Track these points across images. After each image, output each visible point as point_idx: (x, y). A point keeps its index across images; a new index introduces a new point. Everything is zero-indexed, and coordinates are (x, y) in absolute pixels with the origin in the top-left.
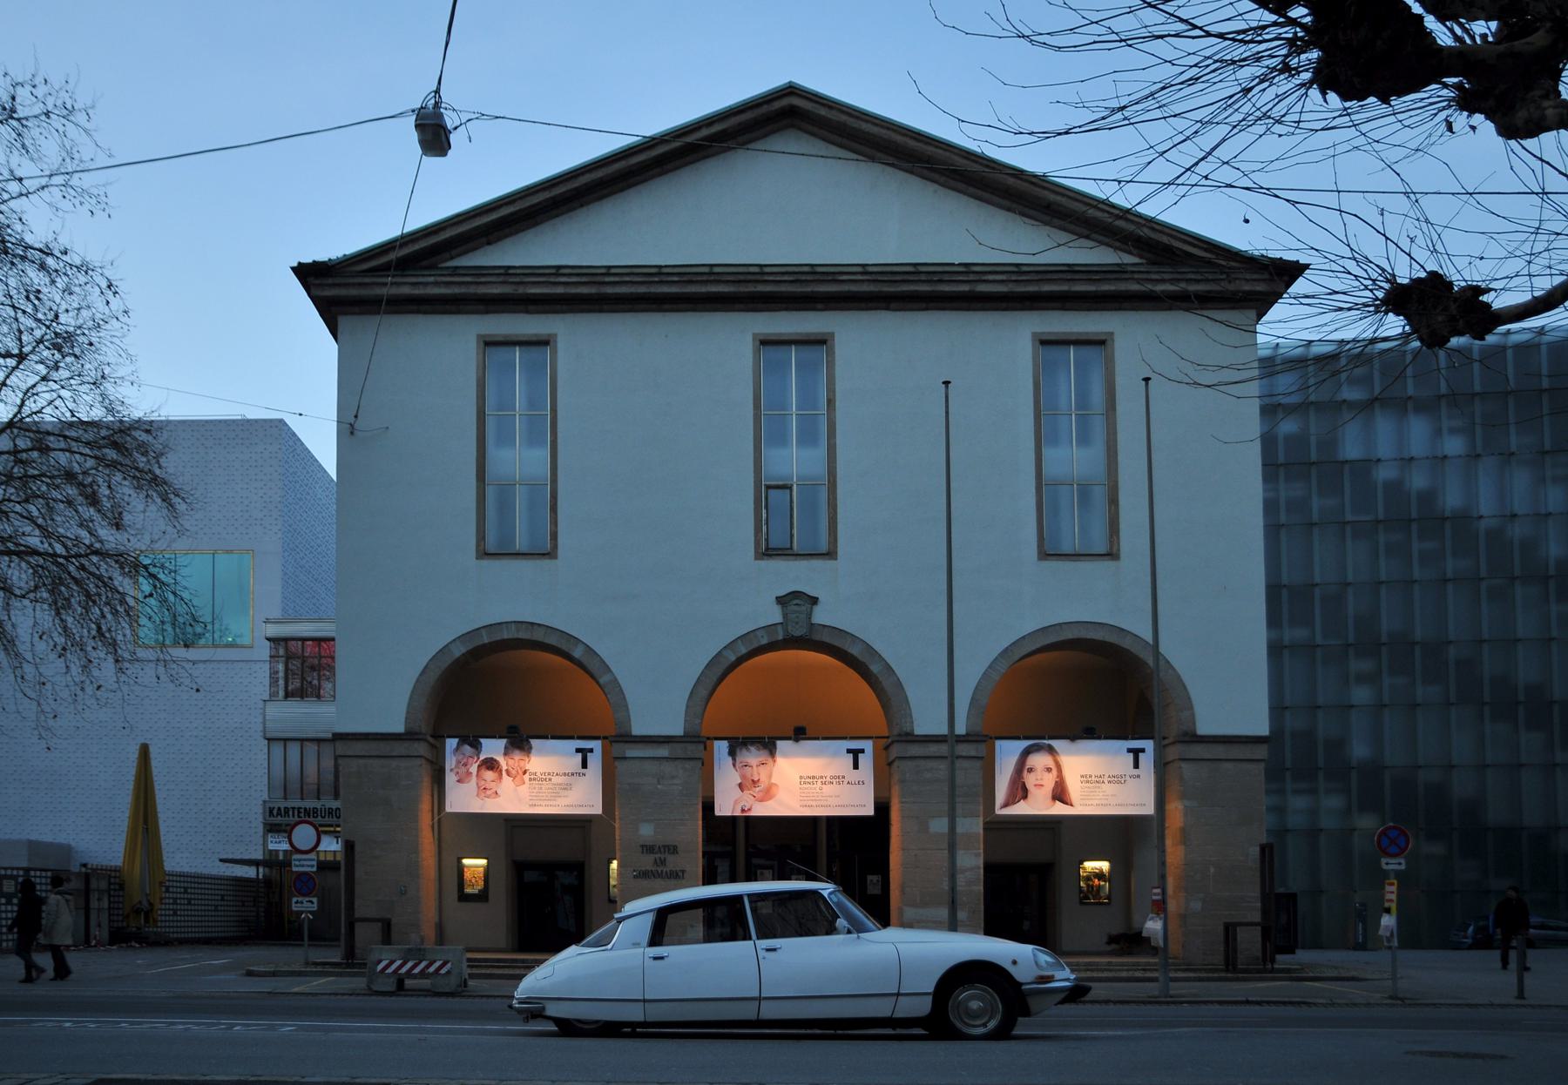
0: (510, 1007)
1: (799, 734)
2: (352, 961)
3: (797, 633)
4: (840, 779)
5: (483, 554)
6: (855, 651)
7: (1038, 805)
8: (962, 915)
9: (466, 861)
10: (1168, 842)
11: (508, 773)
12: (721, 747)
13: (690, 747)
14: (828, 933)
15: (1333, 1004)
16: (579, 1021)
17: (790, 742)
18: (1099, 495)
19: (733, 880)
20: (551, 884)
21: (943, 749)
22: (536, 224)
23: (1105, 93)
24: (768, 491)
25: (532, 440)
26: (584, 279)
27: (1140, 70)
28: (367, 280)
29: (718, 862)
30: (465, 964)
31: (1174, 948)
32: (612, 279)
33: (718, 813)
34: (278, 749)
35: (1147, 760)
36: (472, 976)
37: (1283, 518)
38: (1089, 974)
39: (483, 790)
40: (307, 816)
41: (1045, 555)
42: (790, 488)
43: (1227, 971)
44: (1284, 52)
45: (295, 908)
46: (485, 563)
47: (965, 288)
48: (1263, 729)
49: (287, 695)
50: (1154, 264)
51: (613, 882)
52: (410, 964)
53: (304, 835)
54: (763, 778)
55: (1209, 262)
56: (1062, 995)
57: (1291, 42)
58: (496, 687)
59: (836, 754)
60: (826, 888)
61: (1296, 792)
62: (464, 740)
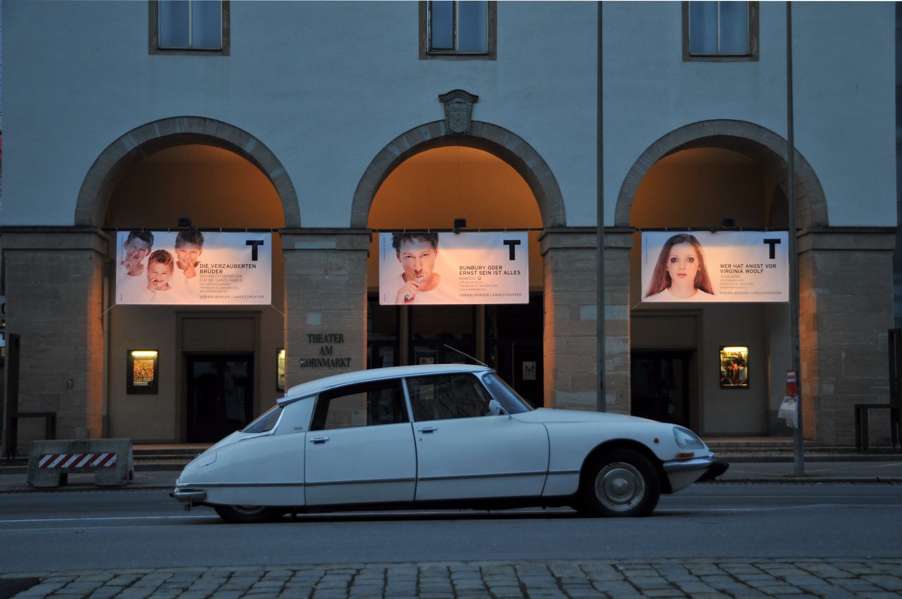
0: (172, 495)
1: (460, 226)
4: (497, 269)
5: (156, 49)
6: (512, 147)
7: (681, 293)
8: (610, 398)
9: (136, 354)
10: (802, 328)
11: (180, 265)
12: (386, 239)
13: (357, 239)
14: (483, 414)
17: (450, 235)
19: (397, 363)
20: (219, 377)
21: (592, 240)
30: (131, 456)
31: (809, 430)
33: (382, 302)
35: (782, 251)
36: (137, 468)
38: (729, 455)
39: (154, 282)
41: (689, 56)
46: (158, 58)
48: (891, 221)
51: (281, 371)
52: (74, 458)
54: (426, 268)
58: (162, 184)
59: (493, 245)
60: (480, 371)
62: (135, 233)
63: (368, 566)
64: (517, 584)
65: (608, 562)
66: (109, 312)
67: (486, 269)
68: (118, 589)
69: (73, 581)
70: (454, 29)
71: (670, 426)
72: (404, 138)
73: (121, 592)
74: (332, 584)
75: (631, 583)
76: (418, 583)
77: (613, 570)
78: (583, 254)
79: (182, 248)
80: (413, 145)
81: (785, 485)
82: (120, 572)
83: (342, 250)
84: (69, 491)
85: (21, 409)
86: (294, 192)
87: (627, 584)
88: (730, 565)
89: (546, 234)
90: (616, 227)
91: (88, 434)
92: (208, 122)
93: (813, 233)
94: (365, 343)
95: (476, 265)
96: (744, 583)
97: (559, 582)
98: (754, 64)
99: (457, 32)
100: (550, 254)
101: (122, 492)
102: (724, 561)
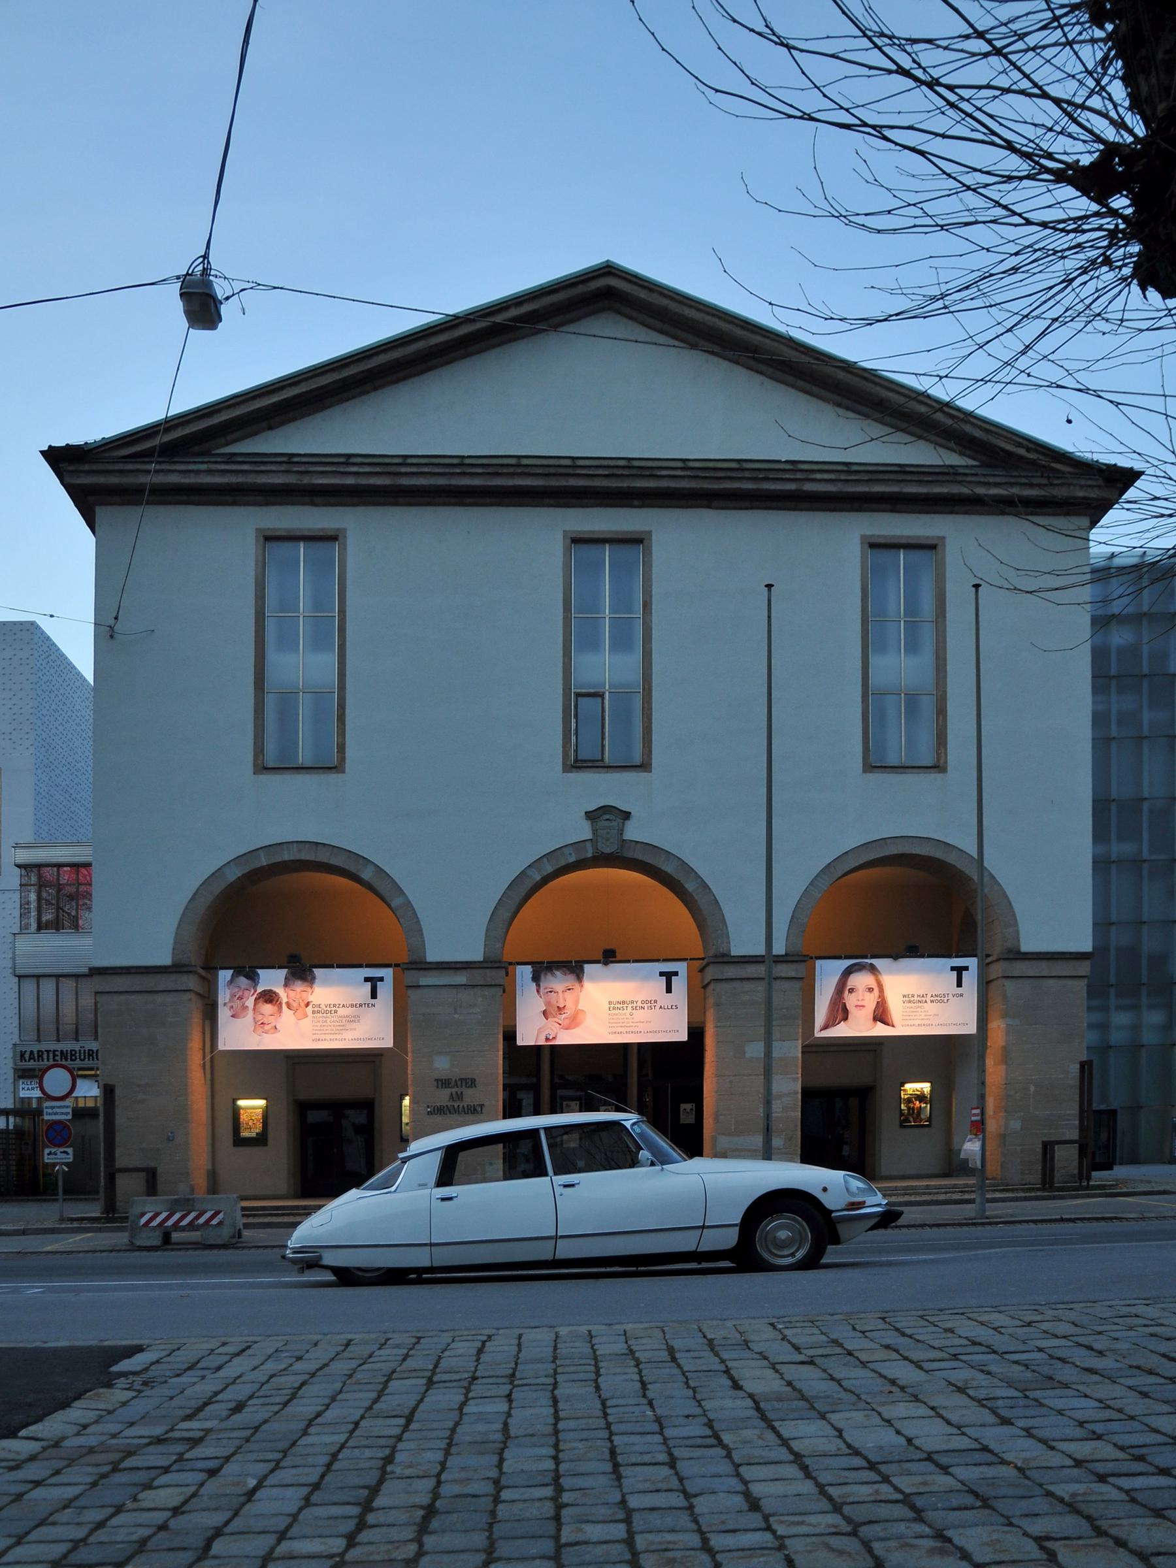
0: (284, 1257)
1: (609, 957)
2: (113, 1215)
3: (608, 851)
4: (651, 1003)
5: (262, 768)
6: (669, 868)
7: (859, 1026)
8: (777, 1142)
9: (242, 1103)
10: (989, 1062)
11: (289, 1005)
12: (524, 973)
13: (493, 973)
15: (1143, 1219)
16: (359, 1269)
18: (927, 705)
19: (537, 1112)
20: (335, 1126)
21: (760, 970)
22: (324, 408)
23: (923, 281)
24: (578, 700)
25: (318, 643)
26: (378, 469)
27: (954, 258)
28: (130, 467)
29: (520, 1095)
30: (239, 1214)
31: (992, 1169)
32: (408, 470)
33: (519, 1042)
34: (29, 987)
35: (970, 978)
36: (246, 1226)
37: (1114, 731)
40: (62, 1059)
41: (870, 767)
42: (602, 696)
43: (1043, 1189)
44: (1105, 243)
45: (47, 1159)
46: (265, 778)
47: (791, 486)
48: (1087, 946)
49: (40, 928)
50: (990, 466)
51: (405, 1120)
52: (177, 1216)
53: (57, 1081)
55: (1033, 463)
56: (872, 1222)
57: (1113, 234)
58: (269, 916)
59: (647, 978)
60: (629, 1119)
61: (1118, 1008)
62: (239, 971)
63: (501, 1332)
64: (664, 1347)
65: (766, 1320)
66: (212, 1058)
67: (639, 1004)
68: (227, 1358)
69: (178, 1349)
70: (603, 739)
71: (841, 1174)
72: (545, 860)
73: (230, 1361)
74: (461, 1351)
75: (789, 1342)
76: (555, 1348)
77: (771, 1328)
78: (748, 986)
79: (292, 987)
80: (556, 867)
81: (965, 1228)
82: (228, 1340)
83: (474, 986)
84: (172, 1250)
85: (118, 1165)
86: (418, 922)
87: (785, 1343)
88: (899, 1319)
89: (708, 964)
90: (786, 955)
91: (192, 1189)
92: (320, 847)
93: (1004, 959)
94: (501, 1087)
95: (628, 999)
96: (910, 1337)
97: (711, 1343)
98: (939, 776)
99: (607, 742)
100: (712, 986)
101: (231, 1251)
102: (891, 1314)
